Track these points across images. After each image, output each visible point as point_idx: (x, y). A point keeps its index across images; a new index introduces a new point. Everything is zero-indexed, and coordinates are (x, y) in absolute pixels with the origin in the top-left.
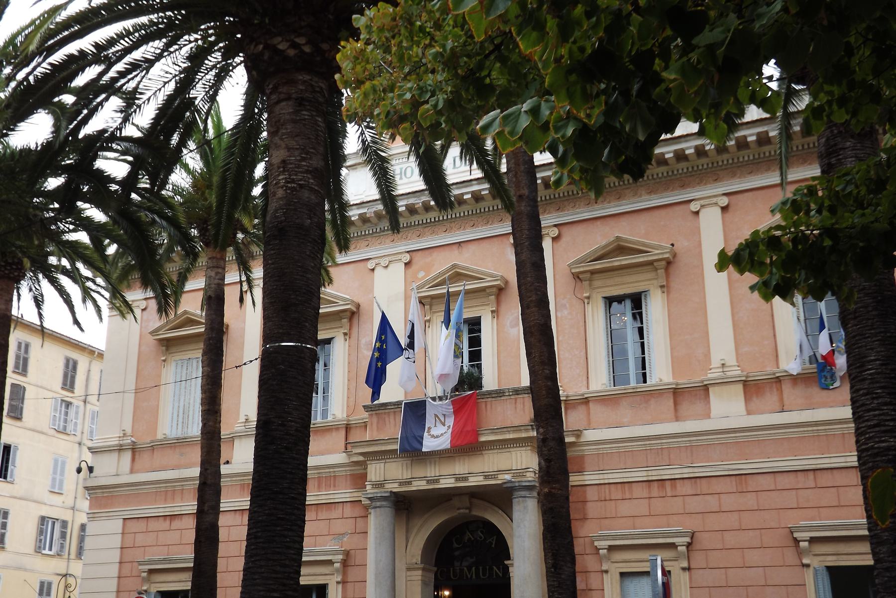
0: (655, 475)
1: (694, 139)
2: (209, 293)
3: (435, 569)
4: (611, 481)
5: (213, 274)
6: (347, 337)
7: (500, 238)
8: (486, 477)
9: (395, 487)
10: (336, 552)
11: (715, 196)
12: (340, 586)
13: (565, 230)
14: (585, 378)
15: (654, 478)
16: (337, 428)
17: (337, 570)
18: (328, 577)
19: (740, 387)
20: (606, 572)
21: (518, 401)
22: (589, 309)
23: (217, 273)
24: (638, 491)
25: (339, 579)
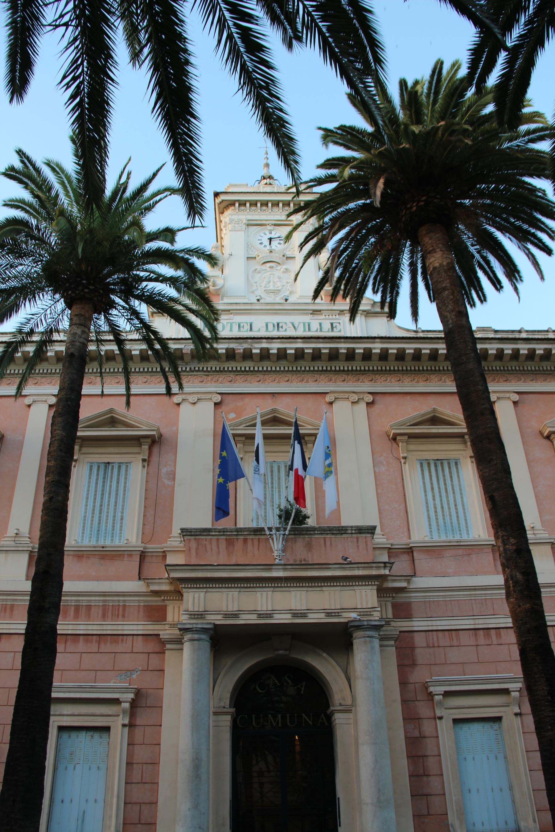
0: (481, 623)
1: (497, 343)
2: (72, 350)
3: (233, 710)
4: (440, 628)
5: (79, 331)
6: (146, 464)
7: (314, 396)
8: (329, 615)
9: (219, 620)
10: (125, 690)
11: (508, 392)
12: (127, 729)
13: (378, 398)
14: (406, 529)
15: (481, 626)
16: (129, 554)
17: (124, 712)
18: (111, 719)
19: (548, 548)
20: (441, 718)
21: (360, 540)
22: (406, 468)
23: (83, 332)
24: (465, 638)
25: (126, 722)
